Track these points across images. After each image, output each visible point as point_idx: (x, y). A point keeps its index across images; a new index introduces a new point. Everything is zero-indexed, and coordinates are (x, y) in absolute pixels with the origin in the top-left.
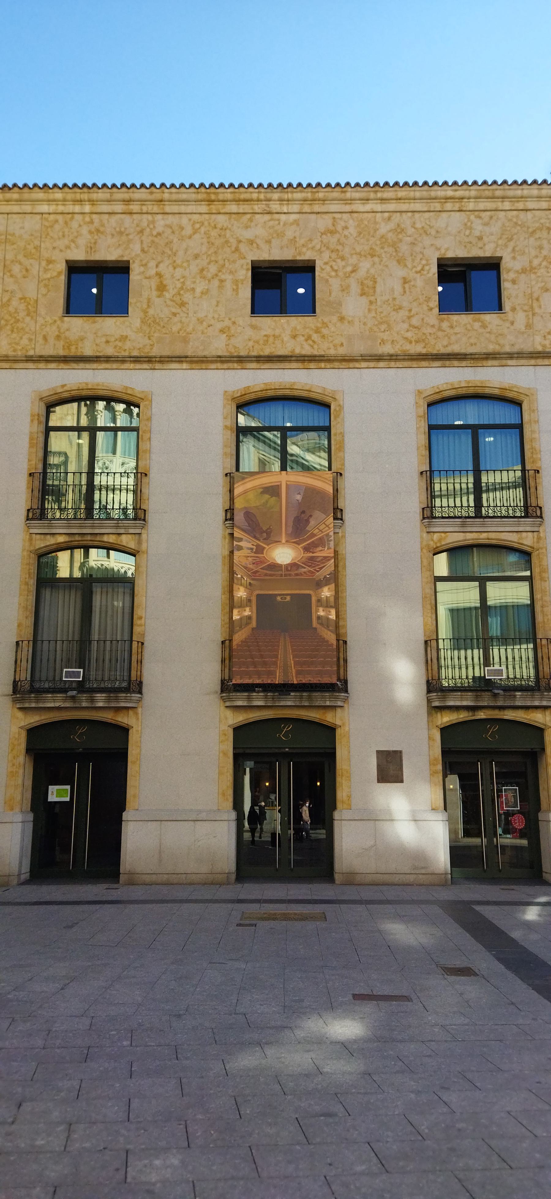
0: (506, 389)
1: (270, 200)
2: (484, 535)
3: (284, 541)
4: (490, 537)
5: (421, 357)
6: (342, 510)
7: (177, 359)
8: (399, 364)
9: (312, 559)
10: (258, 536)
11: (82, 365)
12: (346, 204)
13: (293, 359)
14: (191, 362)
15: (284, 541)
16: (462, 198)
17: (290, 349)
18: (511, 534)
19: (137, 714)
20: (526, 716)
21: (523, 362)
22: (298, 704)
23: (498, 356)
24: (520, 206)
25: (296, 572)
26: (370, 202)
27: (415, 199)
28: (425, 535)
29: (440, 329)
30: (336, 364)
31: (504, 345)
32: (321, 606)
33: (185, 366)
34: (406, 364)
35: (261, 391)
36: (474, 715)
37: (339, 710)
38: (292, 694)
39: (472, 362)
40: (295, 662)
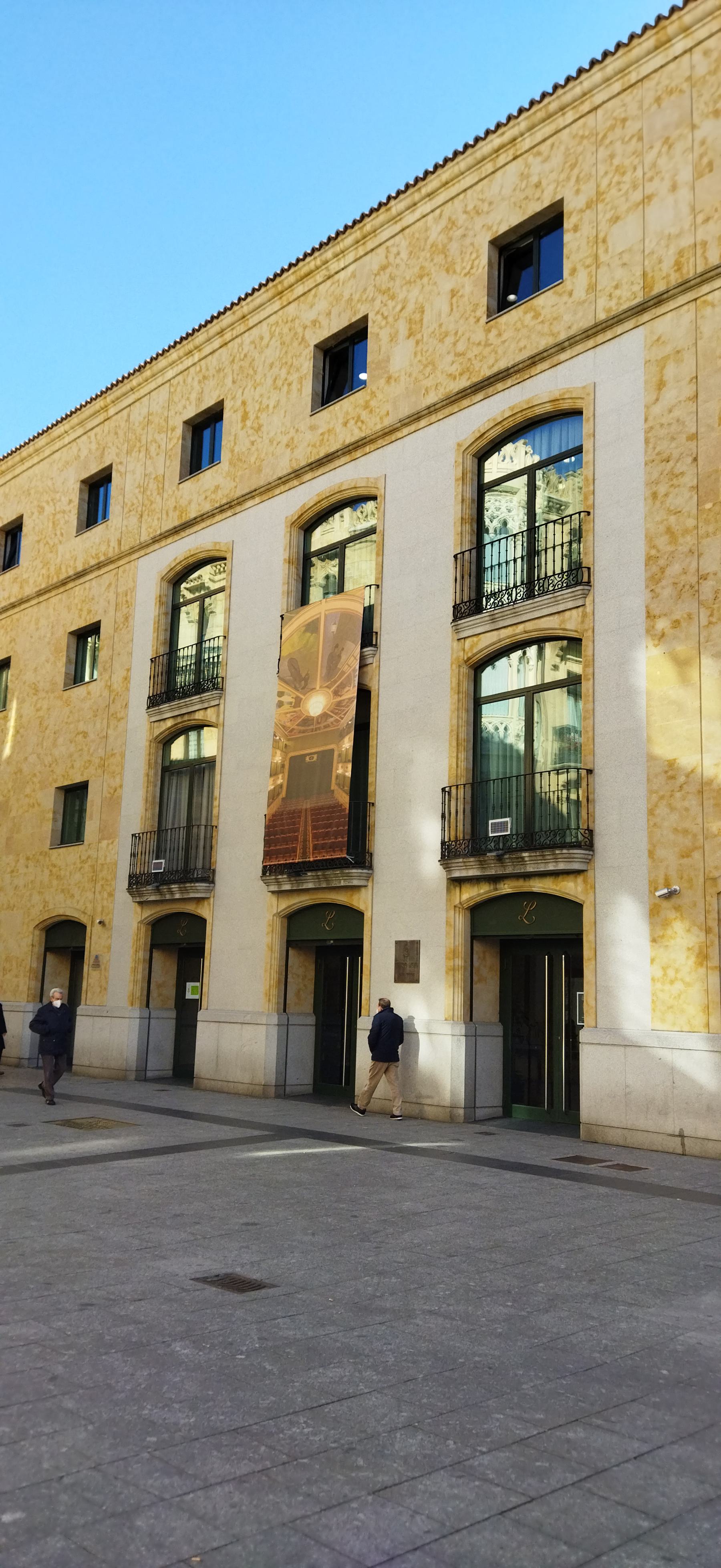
0: (558, 400)
1: (327, 262)
2: (521, 628)
3: (318, 688)
4: (527, 629)
5: (460, 395)
6: (589, 569)
7: (249, 496)
8: (440, 415)
9: (340, 702)
10: (298, 686)
11: (188, 531)
12: (396, 222)
13: (340, 453)
14: (261, 494)
15: (318, 688)
16: (515, 139)
17: (341, 442)
18: (551, 618)
19: (209, 904)
20: (554, 887)
21: (579, 348)
22: (318, 886)
23: (545, 354)
24: (586, 107)
25: (325, 724)
26: (419, 205)
27: (462, 173)
28: (455, 643)
29: (487, 345)
30: (380, 442)
31: (559, 333)
32: (341, 762)
33: (257, 500)
34: (447, 411)
35: (315, 504)
36: (496, 889)
37: (363, 890)
38: (309, 874)
39: (518, 376)
40: (313, 834)
